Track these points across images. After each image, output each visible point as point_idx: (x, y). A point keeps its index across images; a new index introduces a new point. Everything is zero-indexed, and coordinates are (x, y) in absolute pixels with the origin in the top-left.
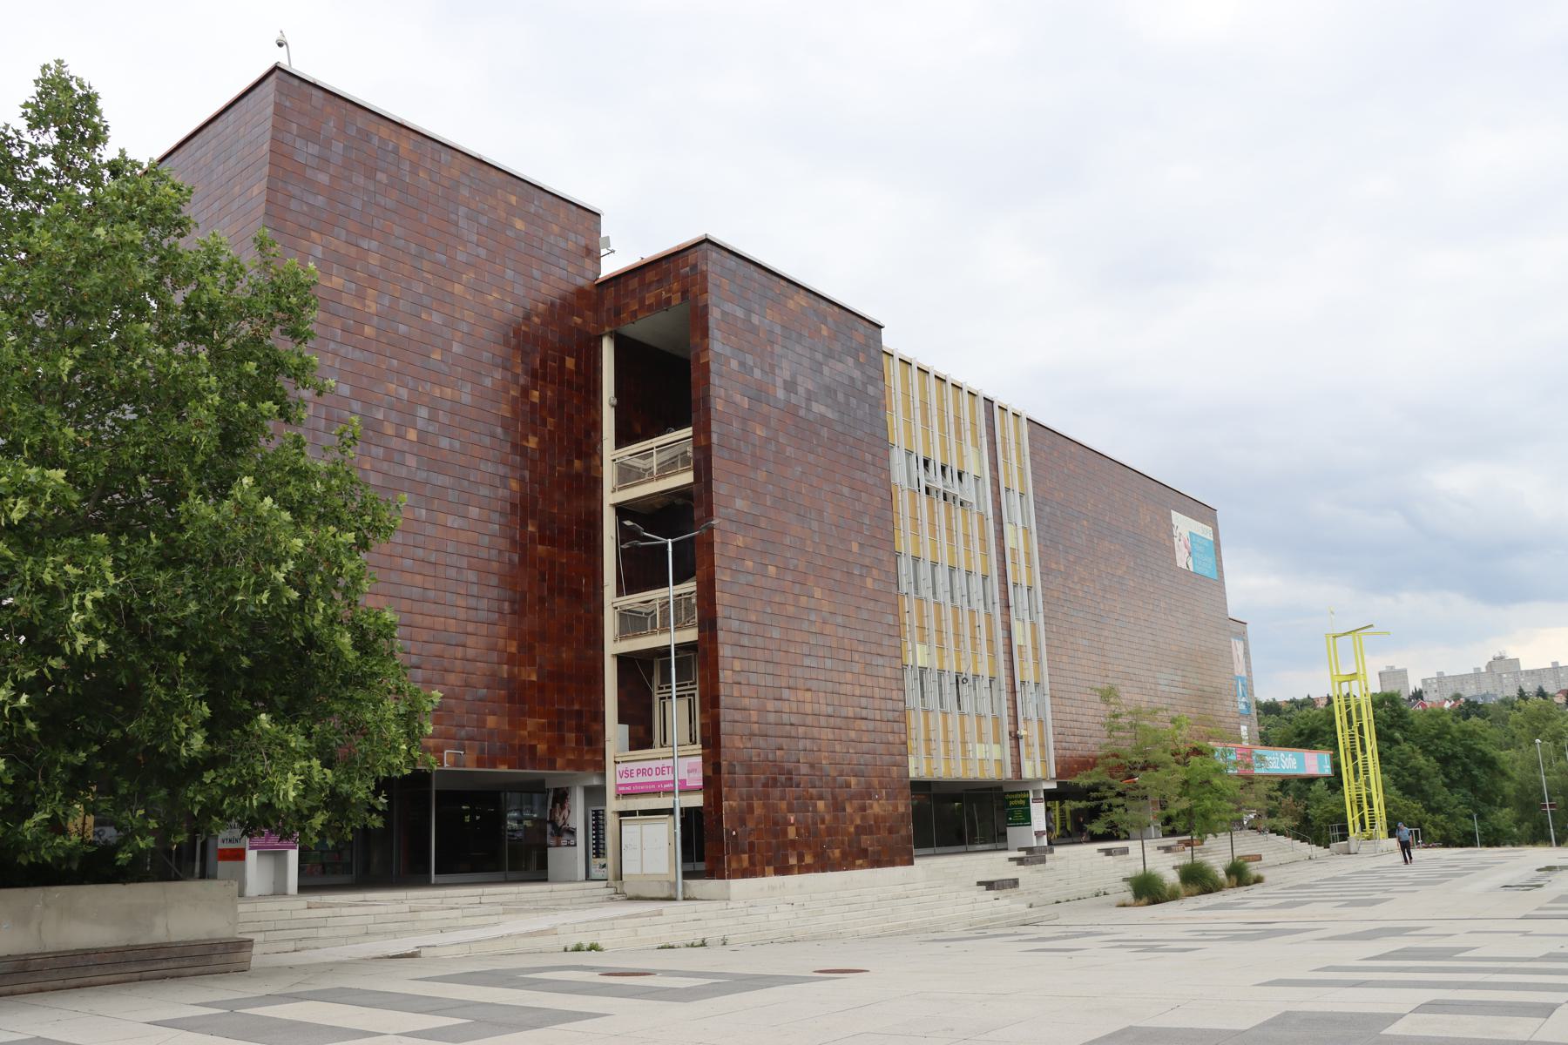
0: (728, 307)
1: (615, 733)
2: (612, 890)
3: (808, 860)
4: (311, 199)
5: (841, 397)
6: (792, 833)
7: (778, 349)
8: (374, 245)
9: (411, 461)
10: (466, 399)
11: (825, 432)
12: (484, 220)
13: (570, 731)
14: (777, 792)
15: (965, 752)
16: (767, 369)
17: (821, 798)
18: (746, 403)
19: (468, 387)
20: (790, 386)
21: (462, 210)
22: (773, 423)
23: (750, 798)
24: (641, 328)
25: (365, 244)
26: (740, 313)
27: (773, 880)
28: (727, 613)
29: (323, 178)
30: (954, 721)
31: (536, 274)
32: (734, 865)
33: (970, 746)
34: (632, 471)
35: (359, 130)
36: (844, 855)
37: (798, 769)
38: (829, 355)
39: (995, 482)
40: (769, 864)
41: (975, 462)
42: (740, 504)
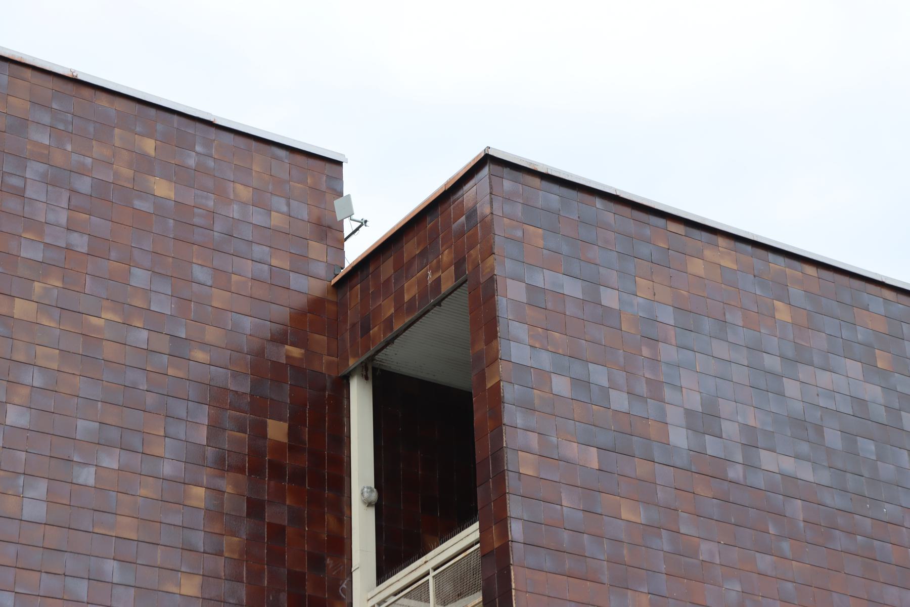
0: (542, 279)
5: (833, 439)
7: (668, 352)
10: (35, 510)
11: (797, 509)
12: (84, 185)
16: (642, 388)
18: (593, 458)
20: (704, 421)
22: (662, 495)
24: (417, 352)
26: (573, 288)
31: (200, 273)
38: (799, 357)
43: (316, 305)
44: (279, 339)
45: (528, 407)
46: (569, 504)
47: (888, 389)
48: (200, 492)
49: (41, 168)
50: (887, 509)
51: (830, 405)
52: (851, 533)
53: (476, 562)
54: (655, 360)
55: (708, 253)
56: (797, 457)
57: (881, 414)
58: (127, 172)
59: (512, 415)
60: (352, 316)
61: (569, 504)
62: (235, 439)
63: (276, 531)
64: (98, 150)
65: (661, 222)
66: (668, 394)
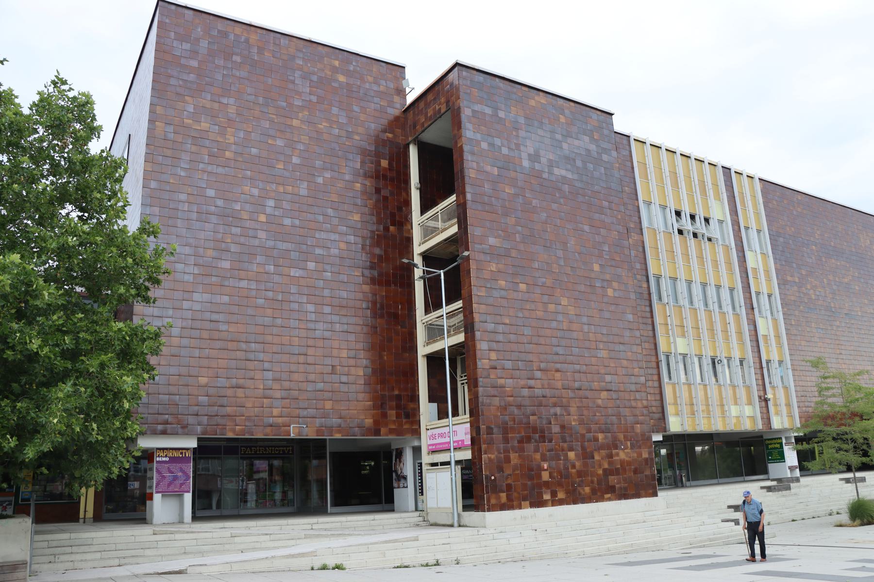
0: (477, 107)
1: (427, 409)
2: (421, 519)
3: (561, 495)
4: (185, 77)
5: (579, 163)
6: (545, 476)
8: (232, 101)
9: (262, 235)
10: (303, 192)
11: (566, 188)
12: (315, 78)
13: (391, 408)
14: (531, 447)
15: (723, 412)
16: (513, 147)
17: (571, 449)
18: (495, 171)
20: (535, 158)
22: (520, 184)
23: (506, 451)
24: (433, 135)
25: (225, 101)
26: (488, 111)
27: (528, 512)
28: (483, 318)
29: (194, 63)
30: (713, 392)
31: (356, 108)
32: (493, 501)
33: (726, 408)
34: (428, 229)
35: (219, 31)
36: (594, 491)
37: (550, 429)
38: (568, 135)
39: (736, 223)
40: (525, 499)
41: (719, 210)
42: (492, 241)
43: (397, 119)
44: (384, 131)
45: (473, 153)
47: (597, 146)
48: (359, 185)
49: (300, 73)
50: (596, 187)
51: (578, 151)
52: (584, 196)
53: (455, 207)
54: (517, 136)
55: (536, 98)
57: (595, 154)
58: (329, 73)
59: (467, 156)
60: (410, 122)
62: (370, 167)
63: (385, 198)
64: (319, 66)
65: (519, 87)
66: (522, 148)
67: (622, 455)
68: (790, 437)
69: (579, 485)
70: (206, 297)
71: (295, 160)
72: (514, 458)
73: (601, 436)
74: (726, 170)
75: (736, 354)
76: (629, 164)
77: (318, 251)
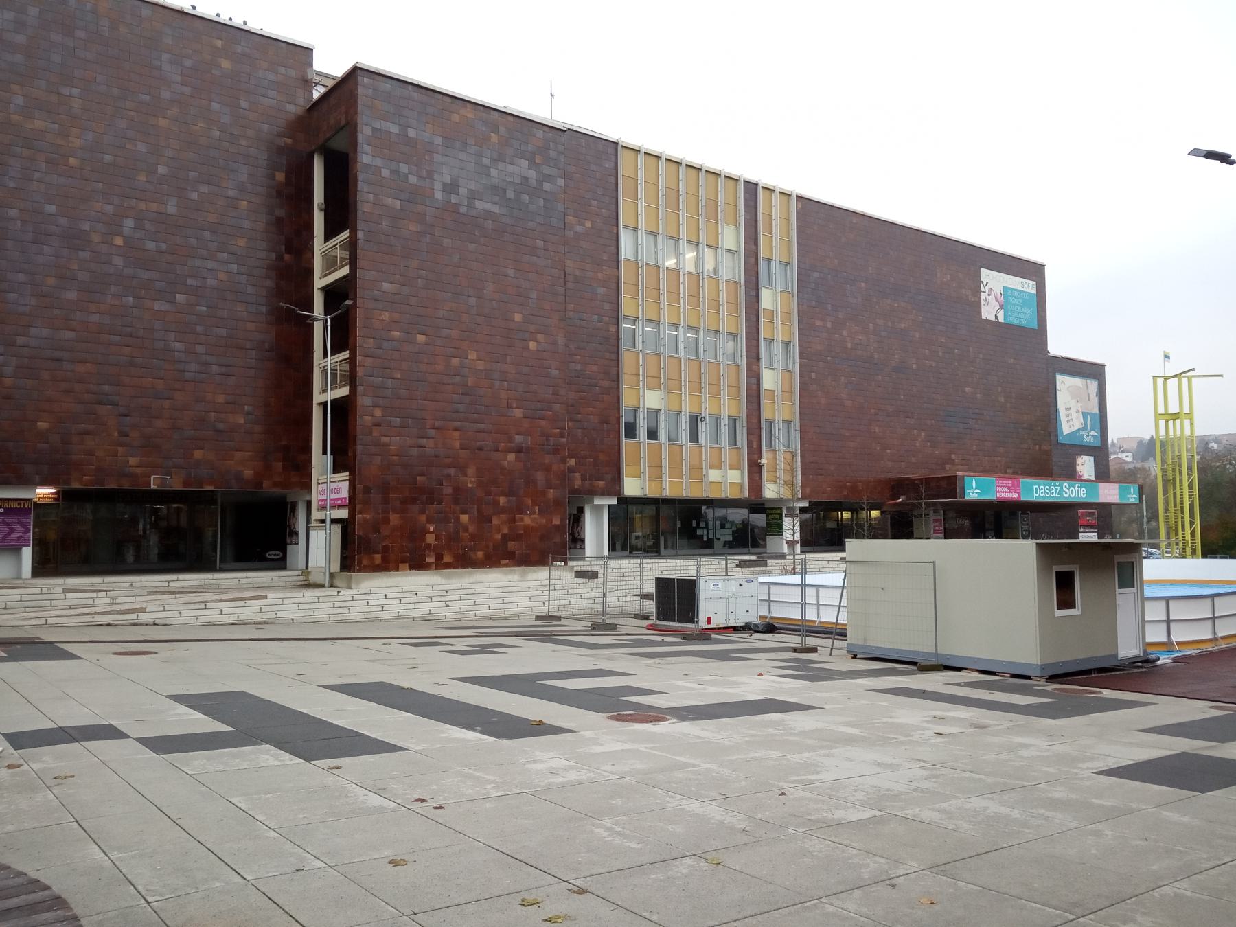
3: (447, 558)
5: (510, 194)
6: (430, 539)
8: (75, 91)
9: (118, 261)
11: (489, 225)
14: (415, 508)
16: (424, 173)
18: (398, 204)
19: (174, 201)
20: (452, 188)
21: (165, 56)
24: (339, 144)
25: (66, 91)
26: (394, 129)
29: (20, 39)
31: (244, 104)
32: (365, 562)
38: (500, 159)
40: (403, 562)
42: (386, 286)
44: (280, 135)
46: (386, 225)
56: (493, 203)
59: (362, 186)
61: (386, 225)
66: (436, 177)
67: (527, 521)
68: (794, 508)
69: (470, 549)
70: (45, 332)
71: (161, 170)
72: (394, 519)
73: (502, 500)
74: (752, 188)
75: (726, 413)
76: (612, 180)
77: (190, 282)
